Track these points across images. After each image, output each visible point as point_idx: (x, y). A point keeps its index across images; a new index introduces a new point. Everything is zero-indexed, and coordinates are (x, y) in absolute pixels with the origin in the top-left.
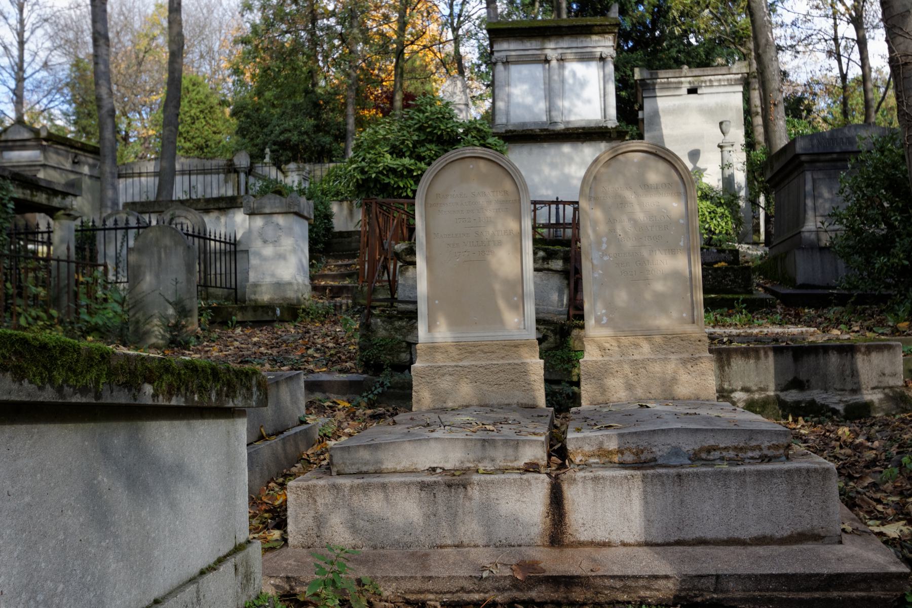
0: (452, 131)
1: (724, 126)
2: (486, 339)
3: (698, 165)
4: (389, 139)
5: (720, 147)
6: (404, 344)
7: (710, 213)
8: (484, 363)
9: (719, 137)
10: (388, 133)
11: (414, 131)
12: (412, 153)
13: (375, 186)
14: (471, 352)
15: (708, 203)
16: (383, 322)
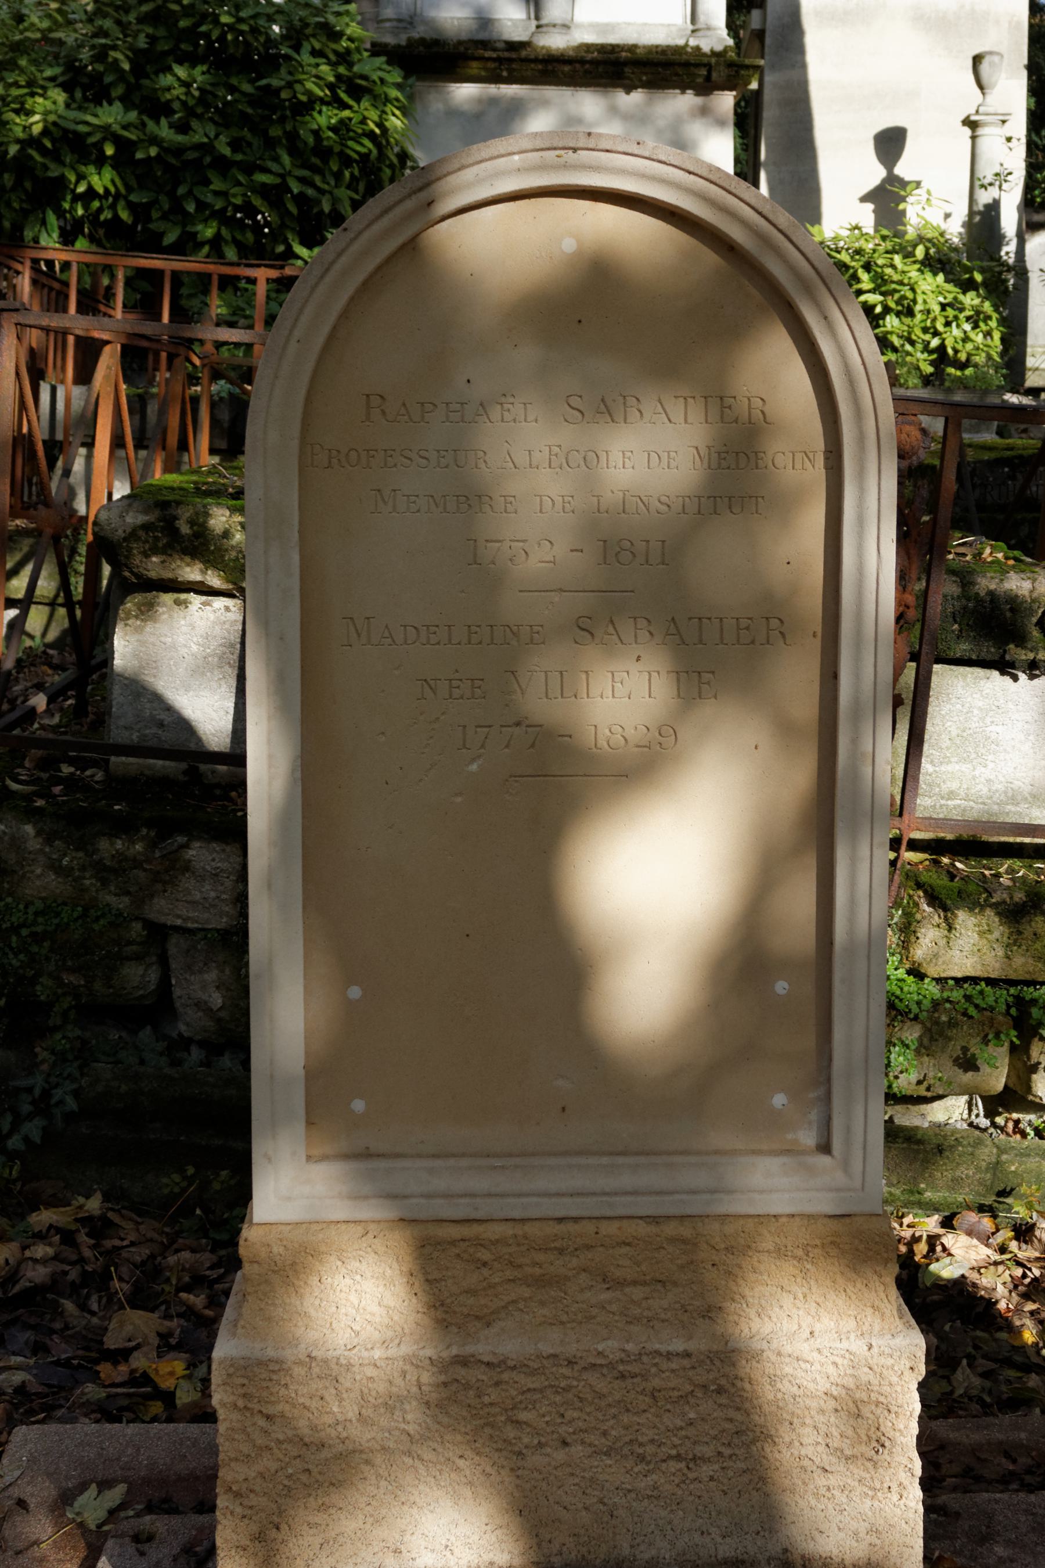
0: (255, 31)
1: (985, 67)
2: (623, 1206)
3: (900, 170)
4: (61, 43)
5: (971, 124)
6: (137, 926)
7: (943, 307)
8: (610, 1346)
9: (967, 98)
10: (56, 26)
11: (140, 20)
12: (131, 89)
13: (18, 184)
14: (541, 1282)
15: (941, 277)
16: (49, 840)
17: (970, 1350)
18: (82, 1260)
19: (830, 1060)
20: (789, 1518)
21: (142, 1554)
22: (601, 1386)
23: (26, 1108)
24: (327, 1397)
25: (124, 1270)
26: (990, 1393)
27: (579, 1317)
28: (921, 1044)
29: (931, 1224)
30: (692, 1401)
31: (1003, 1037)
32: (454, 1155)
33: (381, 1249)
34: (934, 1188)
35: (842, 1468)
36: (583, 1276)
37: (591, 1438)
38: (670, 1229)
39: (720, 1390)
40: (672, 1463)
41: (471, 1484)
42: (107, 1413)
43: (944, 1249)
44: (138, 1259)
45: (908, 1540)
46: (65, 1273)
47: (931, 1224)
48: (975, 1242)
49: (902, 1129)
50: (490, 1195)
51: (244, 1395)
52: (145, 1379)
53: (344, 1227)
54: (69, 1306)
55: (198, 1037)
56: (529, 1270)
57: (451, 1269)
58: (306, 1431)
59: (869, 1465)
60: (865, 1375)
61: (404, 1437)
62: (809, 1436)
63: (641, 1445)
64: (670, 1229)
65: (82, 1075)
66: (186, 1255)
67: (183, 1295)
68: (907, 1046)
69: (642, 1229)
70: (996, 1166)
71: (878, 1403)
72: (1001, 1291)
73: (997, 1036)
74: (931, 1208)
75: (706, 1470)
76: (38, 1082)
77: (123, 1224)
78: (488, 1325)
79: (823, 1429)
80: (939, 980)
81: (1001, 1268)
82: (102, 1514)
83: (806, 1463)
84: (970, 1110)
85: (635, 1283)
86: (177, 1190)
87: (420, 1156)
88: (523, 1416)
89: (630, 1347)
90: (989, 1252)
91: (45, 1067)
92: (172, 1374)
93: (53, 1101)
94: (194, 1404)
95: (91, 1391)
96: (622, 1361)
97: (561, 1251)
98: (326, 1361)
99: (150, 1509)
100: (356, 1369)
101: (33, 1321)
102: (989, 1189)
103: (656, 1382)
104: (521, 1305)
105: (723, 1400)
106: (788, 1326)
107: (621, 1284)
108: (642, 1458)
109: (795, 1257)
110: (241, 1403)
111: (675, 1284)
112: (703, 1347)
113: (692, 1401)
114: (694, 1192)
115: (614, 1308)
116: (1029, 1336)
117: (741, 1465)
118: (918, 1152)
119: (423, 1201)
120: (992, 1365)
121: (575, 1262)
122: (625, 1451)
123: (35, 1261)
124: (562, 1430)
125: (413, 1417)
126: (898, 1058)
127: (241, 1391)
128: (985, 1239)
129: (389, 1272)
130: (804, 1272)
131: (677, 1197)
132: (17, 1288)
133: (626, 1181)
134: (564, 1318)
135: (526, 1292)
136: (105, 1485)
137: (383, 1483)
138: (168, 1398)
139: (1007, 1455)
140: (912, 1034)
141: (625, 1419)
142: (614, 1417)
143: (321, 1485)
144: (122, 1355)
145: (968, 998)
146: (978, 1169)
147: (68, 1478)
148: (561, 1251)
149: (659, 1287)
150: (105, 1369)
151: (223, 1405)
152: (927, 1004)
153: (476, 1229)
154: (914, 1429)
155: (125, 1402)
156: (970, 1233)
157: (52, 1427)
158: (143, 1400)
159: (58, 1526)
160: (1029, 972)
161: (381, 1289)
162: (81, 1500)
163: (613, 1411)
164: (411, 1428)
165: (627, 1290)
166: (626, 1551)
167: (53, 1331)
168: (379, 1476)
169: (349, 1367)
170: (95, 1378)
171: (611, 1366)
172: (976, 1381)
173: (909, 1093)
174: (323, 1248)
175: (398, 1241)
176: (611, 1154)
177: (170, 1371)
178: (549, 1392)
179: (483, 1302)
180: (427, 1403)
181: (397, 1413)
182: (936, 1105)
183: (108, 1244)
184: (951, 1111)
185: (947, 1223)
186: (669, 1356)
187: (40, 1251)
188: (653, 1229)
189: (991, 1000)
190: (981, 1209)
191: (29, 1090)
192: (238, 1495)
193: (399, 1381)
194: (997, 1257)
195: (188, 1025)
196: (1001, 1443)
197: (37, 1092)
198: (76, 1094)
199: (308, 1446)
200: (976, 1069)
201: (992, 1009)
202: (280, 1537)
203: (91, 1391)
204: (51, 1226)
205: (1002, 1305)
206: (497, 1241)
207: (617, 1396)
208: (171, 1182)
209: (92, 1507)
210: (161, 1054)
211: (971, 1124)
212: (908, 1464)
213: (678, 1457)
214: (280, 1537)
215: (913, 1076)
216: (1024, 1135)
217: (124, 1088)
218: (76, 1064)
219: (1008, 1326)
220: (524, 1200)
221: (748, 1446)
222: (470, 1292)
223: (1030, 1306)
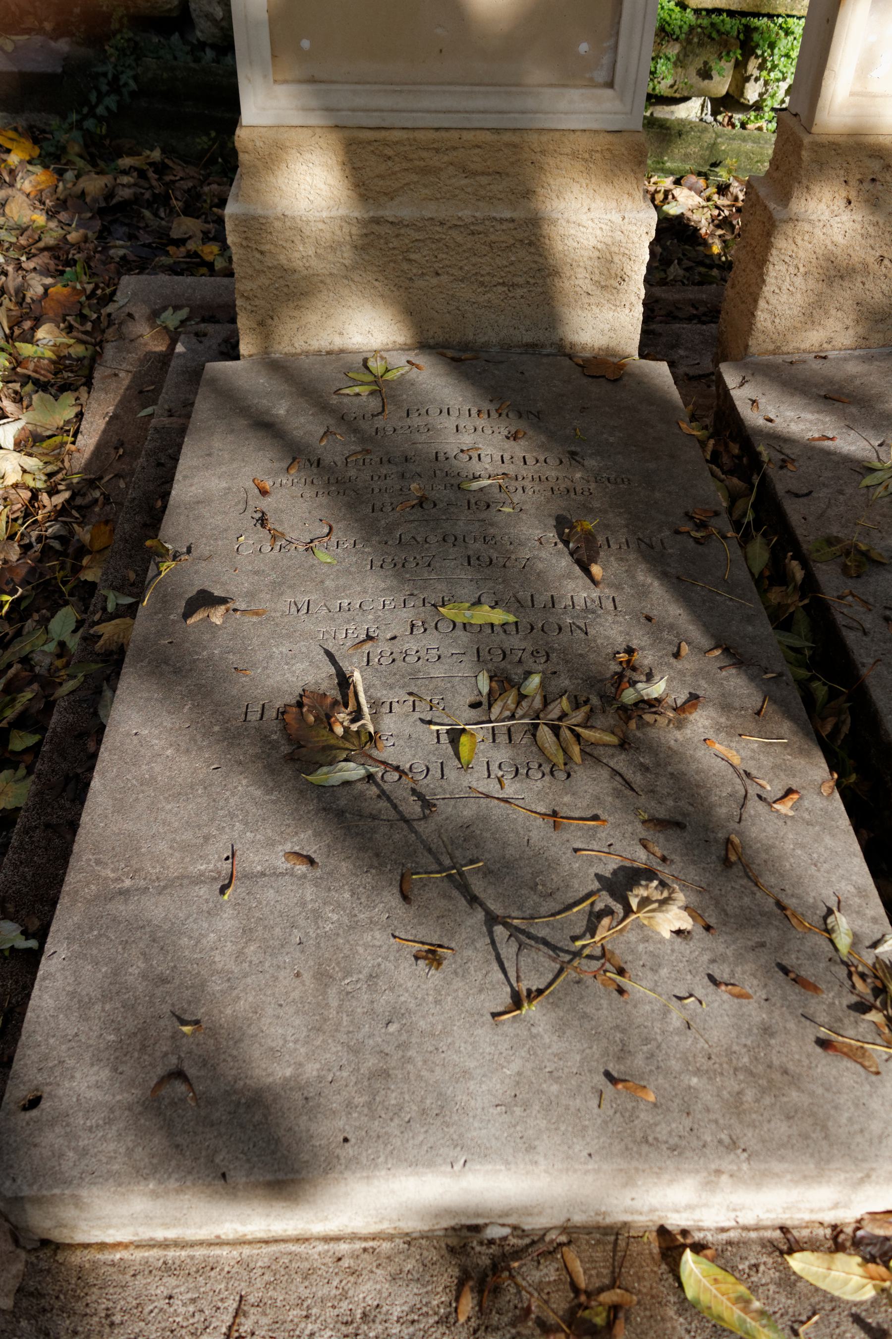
2: (477, 121)
8: (466, 214)
14: (425, 171)
17: (680, 255)
18: (151, 187)
19: (620, 17)
20: (565, 321)
21: (201, 342)
22: (459, 239)
23: (105, 88)
24: (296, 242)
25: (178, 193)
26: (688, 279)
27: (448, 195)
28: (678, 59)
29: (667, 182)
30: (514, 250)
31: (731, 54)
32: (369, 83)
33: (324, 146)
34: (673, 160)
35: (598, 293)
36: (451, 167)
37: (452, 271)
38: (507, 137)
39: (531, 244)
40: (499, 287)
41: (382, 296)
42: (174, 270)
43: (674, 197)
44: (186, 187)
45: (632, 336)
46: (143, 194)
47: (667, 182)
48: (693, 193)
49: (657, 120)
50: (392, 111)
51: (246, 238)
52: (196, 254)
53: (300, 130)
54: (147, 213)
55: (210, 41)
56: (417, 163)
57: (369, 160)
58: (285, 262)
59: (615, 291)
60: (618, 236)
61: (343, 267)
62: (581, 273)
63: (482, 276)
64: (507, 137)
65: (137, 65)
66: (214, 187)
67: (215, 210)
68: (669, 59)
69: (489, 137)
70: (713, 146)
71: (624, 254)
72: (704, 222)
73: (728, 54)
74: (669, 172)
75: (519, 292)
76: (109, 69)
77: (175, 167)
78: (392, 199)
79: (590, 269)
80: (697, 11)
81: (706, 210)
82: (177, 323)
83: (578, 289)
84: (702, 110)
85: (483, 174)
86: (206, 147)
87: (347, 83)
88: (413, 256)
89: (478, 214)
90: (700, 200)
91: (113, 59)
92: (211, 253)
93: (121, 83)
94: (226, 268)
95: (164, 260)
96: (473, 223)
97: (437, 150)
98: (293, 218)
99: (203, 320)
100: (312, 224)
101: (127, 221)
102: (706, 161)
103: (493, 237)
104: (412, 187)
105: (532, 250)
106: (575, 205)
107: (475, 174)
108: (482, 284)
109: (583, 159)
110: (244, 243)
111: (507, 175)
112: (522, 216)
113: (514, 250)
114: (523, 112)
115: (469, 190)
116: (716, 249)
117: (539, 289)
118: (666, 135)
119: (350, 113)
120: (691, 264)
121: (446, 159)
122: (473, 279)
123: (123, 185)
124: (436, 265)
125: (347, 255)
126: (662, 67)
127: (244, 236)
128: (699, 193)
129: (330, 161)
130: (588, 169)
131: (512, 115)
132: (114, 201)
133: (480, 103)
134: (439, 196)
135: (415, 178)
136: (176, 308)
137: (331, 294)
138: (210, 266)
139: (693, 306)
140: (673, 50)
141: (474, 260)
142: (467, 258)
143: (295, 295)
144: (180, 242)
145: (713, 25)
146: (701, 147)
147: (155, 304)
148: (437, 150)
149: (497, 176)
150: (171, 249)
151: (235, 244)
152: (686, 28)
153: (383, 134)
154: (644, 271)
155: (184, 266)
156: (690, 189)
157: (143, 277)
158: (196, 265)
159: (152, 328)
160: (757, 6)
161: (325, 173)
162: (164, 315)
163: (467, 254)
164: (347, 262)
165: (478, 178)
166: (471, 337)
167: (139, 228)
168: (328, 290)
169: (308, 222)
170: (167, 254)
171: (466, 226)
172: (681, 272)
173: (665, 94)
174: (288, 144)
175: (333, 138)
176: (472, 84)
177: (210, 251)
178: (428, 242)
179: (389, 183)
180: (356, 247)
181: (338, 253)
182: (682, 106)
183: (168, 178)
184: (690, 111)
185: (678, 182)
186: (502, 221)
187: (125, 179)
188: (495, 137)
189: (728, 26)
190: (699, 174)
191: (105, 75)
192: (248, 298)
193: (338, 232)
194: (705, 204)
195: (202, 31)
196: (690, 300)
197: (110, 76)
198: (135, 78)
199: (285, 272)
200: (710, 77)
201: (728, 33)
202: (274, 323)
203: (164, 260)
204: (131, 167)
205: (703, 231)
206: (397, 142)
207: (469, 245)
208: (202, 142)
209: (171, 319)
210: (187, 53)
211: (701, 120)
212: (636, 290)
213: (503, 284)
214: (274, 323)
215: (669, 81)
216: (734, 126)
217: (165, 75)
218: (133, 57)
219: (705, 244)
220: (414, 115)
221: (544, 278)
222: (381, 177)
223: (720, 232)
